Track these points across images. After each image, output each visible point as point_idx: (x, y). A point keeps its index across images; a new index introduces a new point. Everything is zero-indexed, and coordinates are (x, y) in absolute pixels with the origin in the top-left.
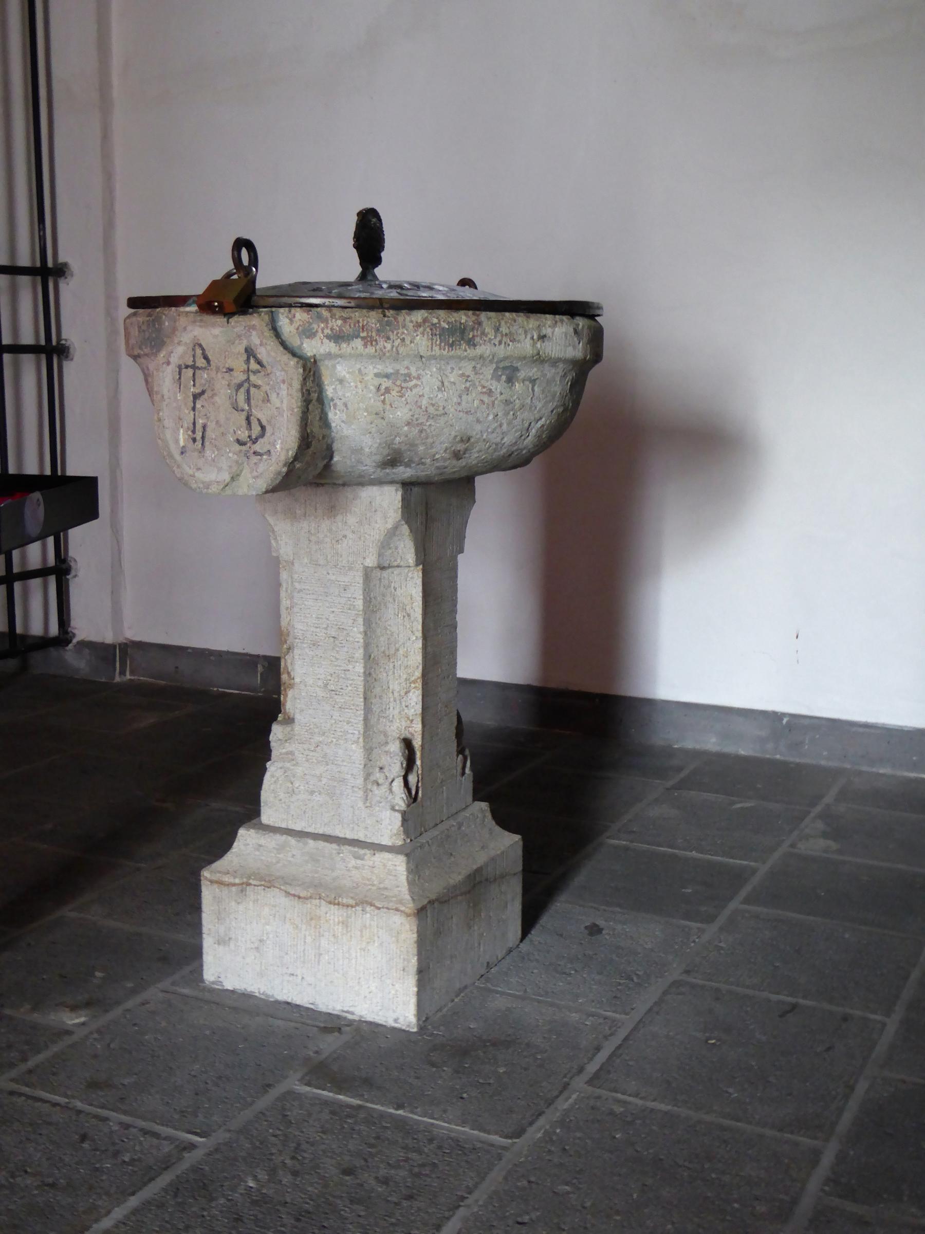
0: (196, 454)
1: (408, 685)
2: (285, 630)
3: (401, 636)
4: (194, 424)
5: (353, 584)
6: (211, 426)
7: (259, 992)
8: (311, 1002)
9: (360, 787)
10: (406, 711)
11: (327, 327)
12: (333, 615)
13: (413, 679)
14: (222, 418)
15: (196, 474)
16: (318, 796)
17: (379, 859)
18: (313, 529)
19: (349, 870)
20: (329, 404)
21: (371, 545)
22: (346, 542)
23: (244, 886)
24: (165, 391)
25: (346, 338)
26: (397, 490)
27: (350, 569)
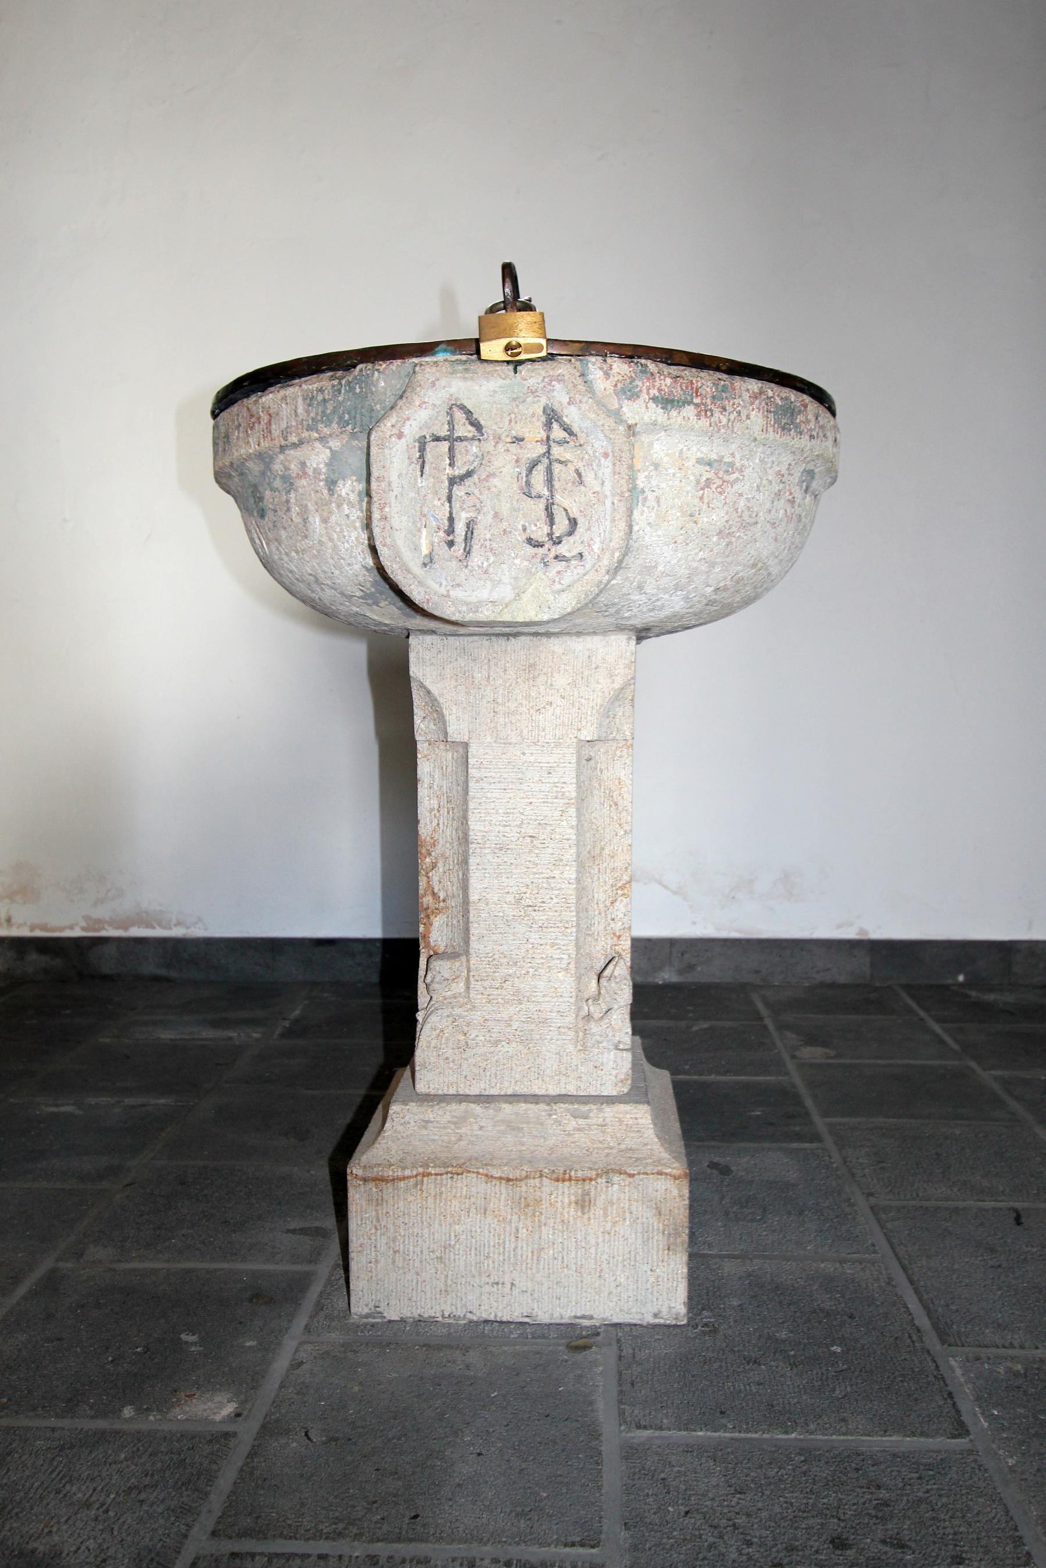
0: (454, 563)
1: (615, 892)
2: (428, 839)
3: (607, 830)
4: (451, 519)
5: (562, 765)
6: (484, 521)
7: (443, 1316)
8: (525, 1314)
9: (571, 1026)
10: (612, 925)
11: (654, 386)
12: (531, 807)
13: (620, 884)
14: (505, 509)
15: (452, 593)
16: (507, 1045)
17: (611, 1114)
18: (500, 697)
19: (569, 1135)
20: (638, 497)
21: (589, 713)
22: (551, 711)
23: (419, 1178)
24: (394, 477)
25: (675, 403)
26: (629, 639)
27: (558, 745)
